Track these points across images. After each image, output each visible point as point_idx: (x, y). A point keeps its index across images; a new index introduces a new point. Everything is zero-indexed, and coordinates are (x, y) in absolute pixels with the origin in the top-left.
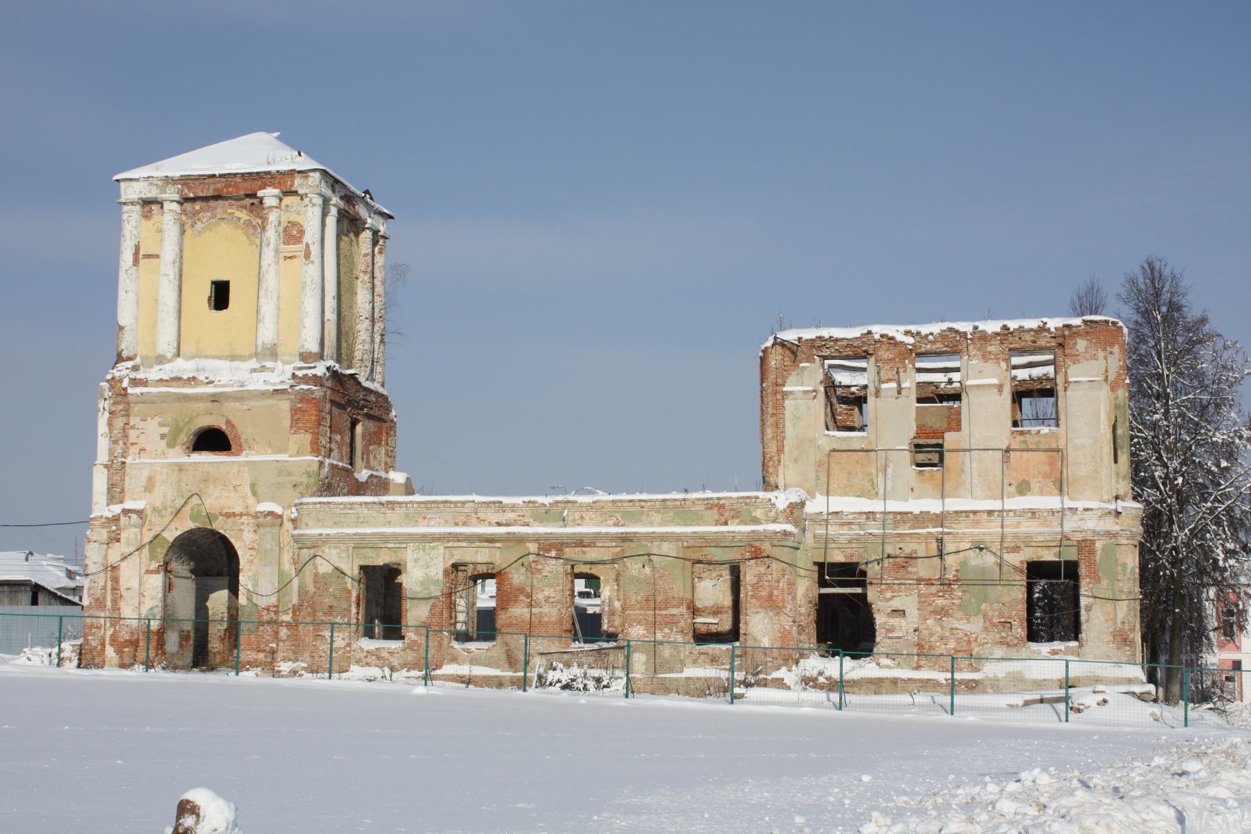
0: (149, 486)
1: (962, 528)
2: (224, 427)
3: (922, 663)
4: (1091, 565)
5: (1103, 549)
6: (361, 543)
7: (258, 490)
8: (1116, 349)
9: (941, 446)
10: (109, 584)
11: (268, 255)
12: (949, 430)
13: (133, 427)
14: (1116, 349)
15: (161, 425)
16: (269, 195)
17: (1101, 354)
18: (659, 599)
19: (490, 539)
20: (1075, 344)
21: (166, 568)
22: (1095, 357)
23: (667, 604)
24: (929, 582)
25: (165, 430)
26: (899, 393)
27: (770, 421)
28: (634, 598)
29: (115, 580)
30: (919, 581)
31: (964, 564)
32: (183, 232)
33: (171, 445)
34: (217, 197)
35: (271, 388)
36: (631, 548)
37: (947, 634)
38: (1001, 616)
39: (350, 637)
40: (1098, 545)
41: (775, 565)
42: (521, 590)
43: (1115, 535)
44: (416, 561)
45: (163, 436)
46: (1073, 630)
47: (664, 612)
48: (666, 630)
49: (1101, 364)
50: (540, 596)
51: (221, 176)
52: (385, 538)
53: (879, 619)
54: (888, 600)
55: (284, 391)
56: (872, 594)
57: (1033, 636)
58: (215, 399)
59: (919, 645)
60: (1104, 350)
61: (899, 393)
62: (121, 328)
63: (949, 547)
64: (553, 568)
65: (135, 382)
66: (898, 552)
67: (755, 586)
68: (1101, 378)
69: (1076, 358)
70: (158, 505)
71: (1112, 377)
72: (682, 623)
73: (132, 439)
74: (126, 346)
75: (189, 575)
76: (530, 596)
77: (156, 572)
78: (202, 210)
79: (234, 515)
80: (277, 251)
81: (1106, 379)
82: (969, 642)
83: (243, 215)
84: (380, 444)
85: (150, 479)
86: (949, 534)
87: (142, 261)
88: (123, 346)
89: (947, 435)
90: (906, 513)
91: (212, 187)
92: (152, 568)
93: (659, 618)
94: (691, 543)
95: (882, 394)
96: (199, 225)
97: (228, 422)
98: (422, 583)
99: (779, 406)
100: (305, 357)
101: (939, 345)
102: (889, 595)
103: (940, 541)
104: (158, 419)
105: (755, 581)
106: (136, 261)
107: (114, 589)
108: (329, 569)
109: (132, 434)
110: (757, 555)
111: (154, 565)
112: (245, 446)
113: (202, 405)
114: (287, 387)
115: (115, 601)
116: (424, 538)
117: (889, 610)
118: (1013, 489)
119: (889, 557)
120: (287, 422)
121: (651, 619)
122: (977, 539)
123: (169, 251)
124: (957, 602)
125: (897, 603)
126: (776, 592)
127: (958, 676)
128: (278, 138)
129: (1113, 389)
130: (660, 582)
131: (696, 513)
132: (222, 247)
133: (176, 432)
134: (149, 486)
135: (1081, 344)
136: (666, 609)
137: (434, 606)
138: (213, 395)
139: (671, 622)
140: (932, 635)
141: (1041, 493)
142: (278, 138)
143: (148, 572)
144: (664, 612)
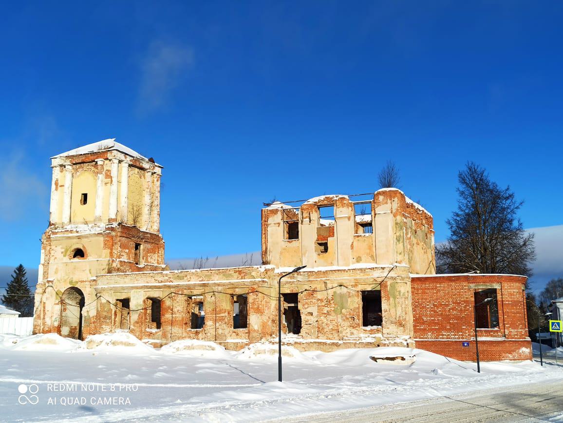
0: (56, 273)
1: (332, 277)
2: (82, 248)
3: (319, 335)
4: (386, 291)
5: (390, 285)
6: (116, 290)
7: (91, 271)
8: (396, 199)
9: (327, 243)
10: (42, 309)
11: (99, 182)
12: (330, 236)
13: (53, 250)
14: (396, 199)
15: (62, 248)
16: (100, 161)
17: (389, 201)
18: (217, 310)
19: (159, 287)
20: (378, 198)
21: (62, 302)
22: (386, 203)
23: (221, 311)
24: (321, 300)
25: (63, 250)
26: (310, 222)
27: (264, 236)
28: (208, 309)
29: (44, 307)
30: (319, 300)
31: (335, 292)
32: (73, 176)
33: (64, 256)
34: (83, 163)
35: (97, 233)
36: (207, 289)
37: (329, 322)
38: (350, 314)
39: (112, 328)
40: (389, 283)
41: (260, 295)
42: (169, 307)
43: (395, 279)
44: (134, 297)
45: (62, 253)
46: (378, 321)
47: (219, 315)
48: (220, 323)
49: (389, 205)
50: (175, 310)
51: (84, 154)
52: (123, 288)
53: (303, 317)
54: (306, 308)
55: (101, 234)
56: (300, 307)
57: (365, 324)
58: (79, 238)
59: (318, 327)
60: (391, 199)
61: (310, 222)
62: (51, 213)
63: (329, 286)
64: (181, 299)
65: (54, 233)
66: (310, 288)
67: (253, 303)
68: (390, 212)
69: (379, 204)
70: (59, 279)
71: (394, 211)
72: (226, 320)
73: (52, 254)
74: (53, 220)
75: (75, 305)
76: (172, 310)
77: (58, 304)
78: (79, 168)
79: (83, 281)
80: (102, 181)
81: (392, 212)
82: (337, 326)
83: (93, 168)
84: (155, 253)
85: (57, 269)
86: (329, 280)
87: (59, 188)
88: (51, 220)
89: (329, 239)
90: (312, 272)
91: (81, 159)
92: (56, 303)
93: (217, 318)
94: (229, 286)
95: (304, 223)
96: (78, 173)
97: (84, 247)
98: (136, 306)
99: (266, 230)
100: (110, 220)
101: (325, 202)
102: (306, 306)
103: (325, 283)
104: (61, 246)
105: (252, 302)
106: (56, 189)
107: (44, 311)
108: (105, 301)
109: (52, 252)
110: (254, 291)
111: (57, 302)
112: (88, 255)
113: (75, 240)
114: (102, 232)
115: (44, 315)
116: (137, 288)
117: (306, 313)
118: (355, 260)
119: (306, 290)
120: (102, 245)
121: (214, 318)
122: (340, 281)
123: (67, 183)
124: (333, 309)
125: (309, 310)
126: (260, 306)
127: (479, 339)
128: (115, 141)
129: (395, 216)
130: (218, 303)
131: (230, 274)
132: (86, 180)
133: (66, 251)
134: (56, 273)
135: (381, 198)
136: (220, 314)
137: (140, 315)
138: (78, 236)
139: (222, 319)
140: (323, 323)
141: (366, 262)
142: (115, 141)
143: (55, 304)
144: (219, 315)
